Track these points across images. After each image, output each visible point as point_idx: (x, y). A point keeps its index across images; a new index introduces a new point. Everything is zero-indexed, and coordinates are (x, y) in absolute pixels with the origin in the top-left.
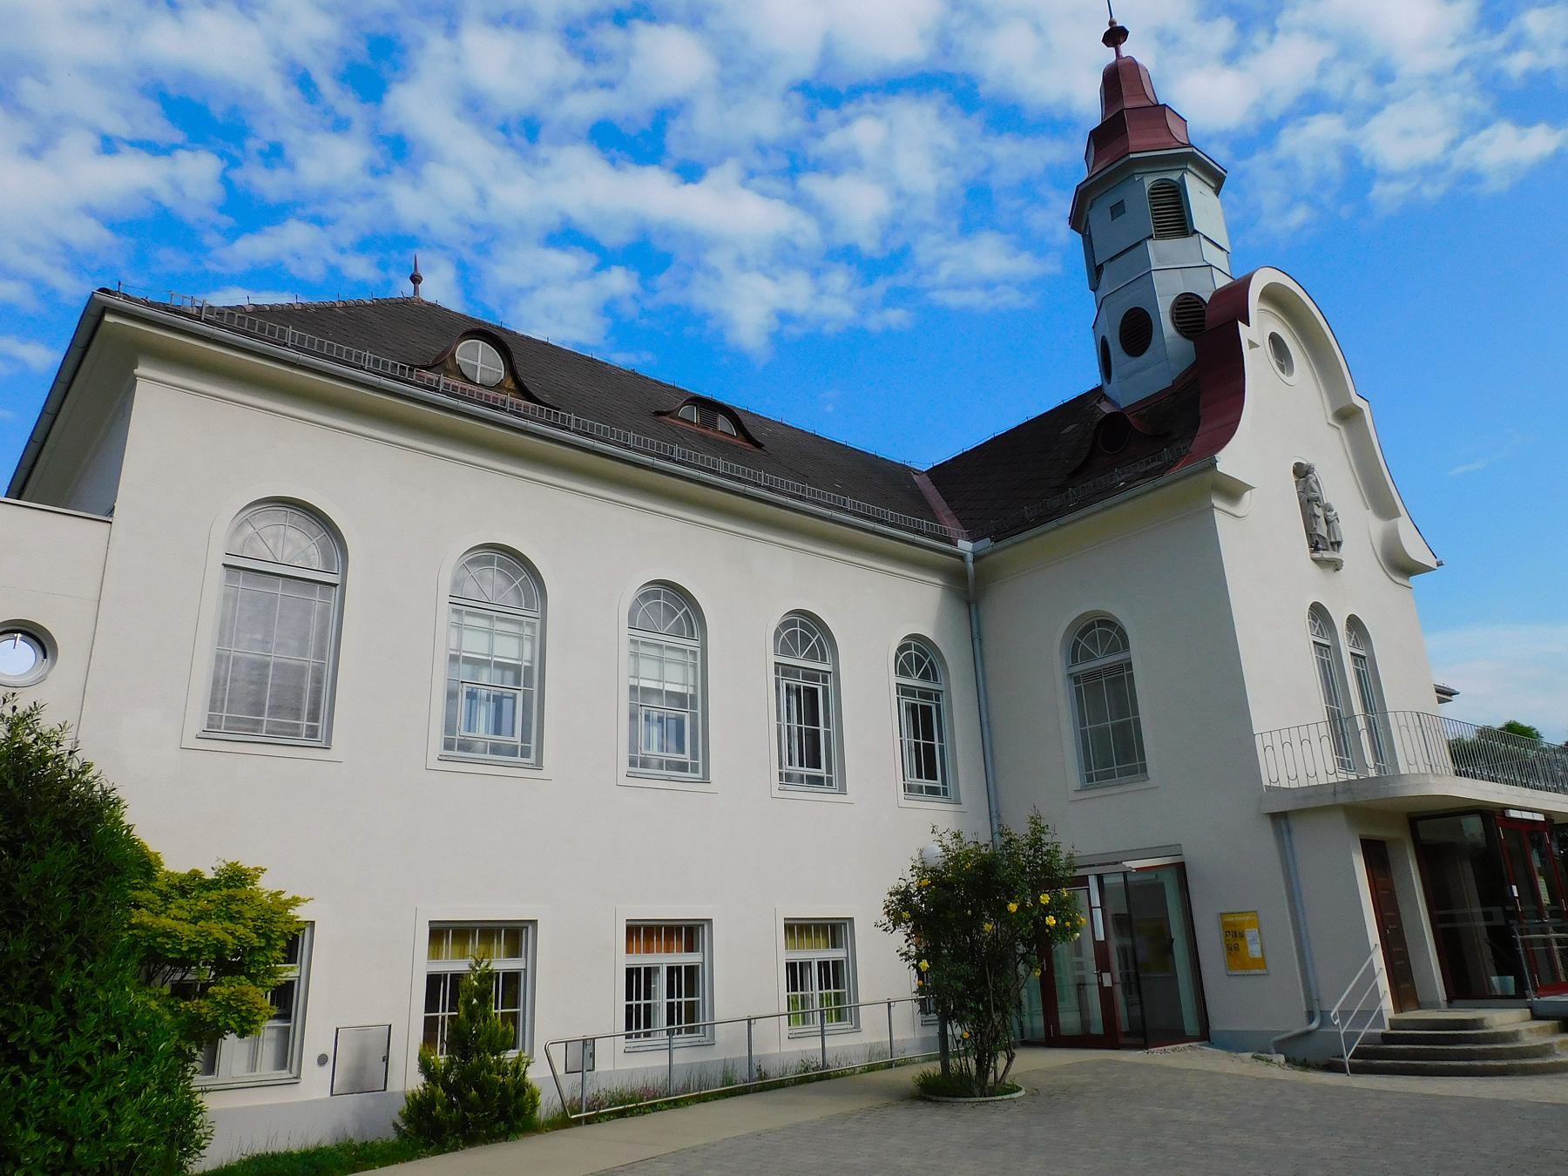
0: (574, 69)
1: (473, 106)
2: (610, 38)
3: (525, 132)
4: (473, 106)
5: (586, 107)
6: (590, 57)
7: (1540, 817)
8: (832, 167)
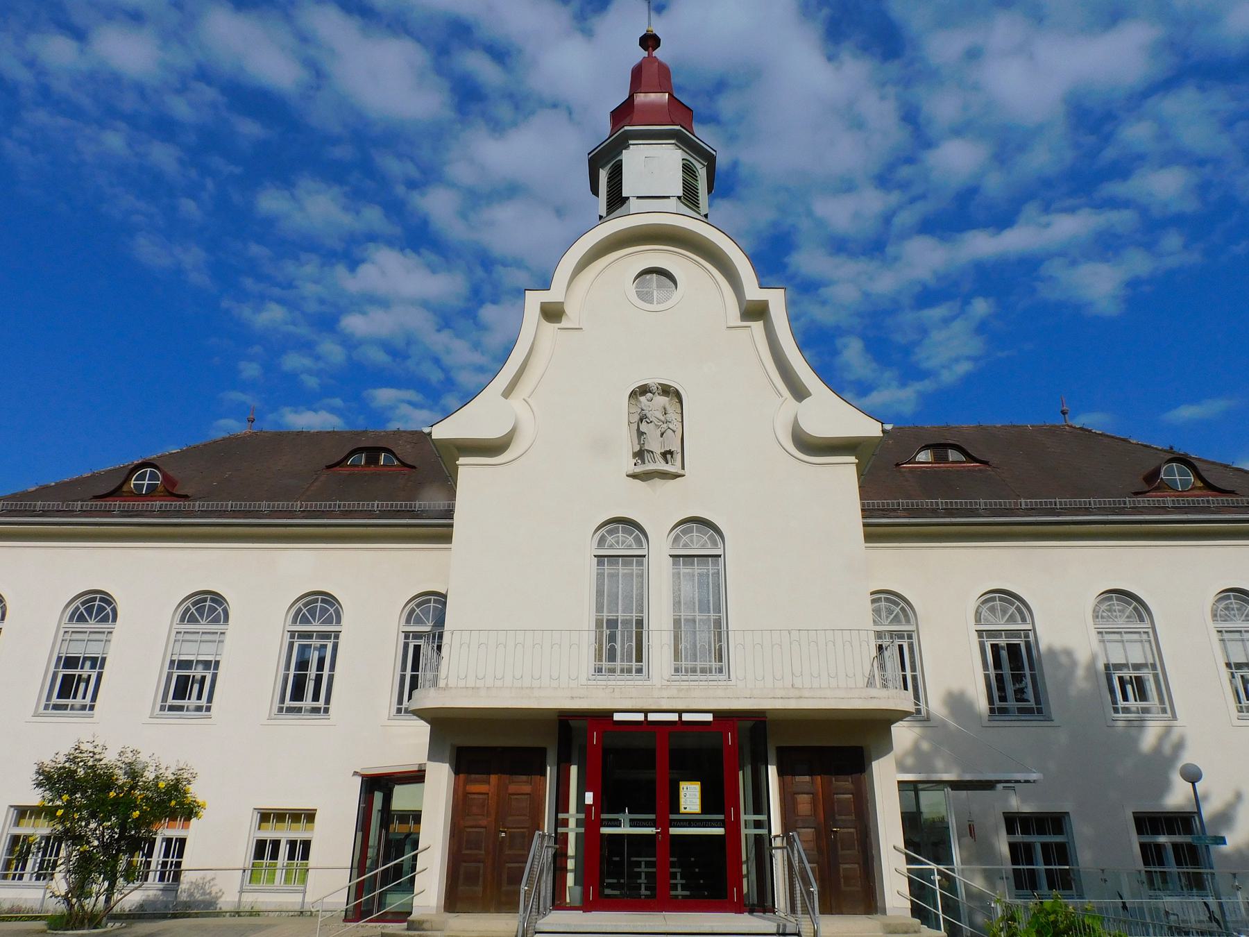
0: (894, 198)
1: (840, 246)
2: (905, 172)
3: (876, 246)
4: (840, 246)
5: (906, 218)
6: (904, 186)
7: (709, 717)
8: (1122, 169)
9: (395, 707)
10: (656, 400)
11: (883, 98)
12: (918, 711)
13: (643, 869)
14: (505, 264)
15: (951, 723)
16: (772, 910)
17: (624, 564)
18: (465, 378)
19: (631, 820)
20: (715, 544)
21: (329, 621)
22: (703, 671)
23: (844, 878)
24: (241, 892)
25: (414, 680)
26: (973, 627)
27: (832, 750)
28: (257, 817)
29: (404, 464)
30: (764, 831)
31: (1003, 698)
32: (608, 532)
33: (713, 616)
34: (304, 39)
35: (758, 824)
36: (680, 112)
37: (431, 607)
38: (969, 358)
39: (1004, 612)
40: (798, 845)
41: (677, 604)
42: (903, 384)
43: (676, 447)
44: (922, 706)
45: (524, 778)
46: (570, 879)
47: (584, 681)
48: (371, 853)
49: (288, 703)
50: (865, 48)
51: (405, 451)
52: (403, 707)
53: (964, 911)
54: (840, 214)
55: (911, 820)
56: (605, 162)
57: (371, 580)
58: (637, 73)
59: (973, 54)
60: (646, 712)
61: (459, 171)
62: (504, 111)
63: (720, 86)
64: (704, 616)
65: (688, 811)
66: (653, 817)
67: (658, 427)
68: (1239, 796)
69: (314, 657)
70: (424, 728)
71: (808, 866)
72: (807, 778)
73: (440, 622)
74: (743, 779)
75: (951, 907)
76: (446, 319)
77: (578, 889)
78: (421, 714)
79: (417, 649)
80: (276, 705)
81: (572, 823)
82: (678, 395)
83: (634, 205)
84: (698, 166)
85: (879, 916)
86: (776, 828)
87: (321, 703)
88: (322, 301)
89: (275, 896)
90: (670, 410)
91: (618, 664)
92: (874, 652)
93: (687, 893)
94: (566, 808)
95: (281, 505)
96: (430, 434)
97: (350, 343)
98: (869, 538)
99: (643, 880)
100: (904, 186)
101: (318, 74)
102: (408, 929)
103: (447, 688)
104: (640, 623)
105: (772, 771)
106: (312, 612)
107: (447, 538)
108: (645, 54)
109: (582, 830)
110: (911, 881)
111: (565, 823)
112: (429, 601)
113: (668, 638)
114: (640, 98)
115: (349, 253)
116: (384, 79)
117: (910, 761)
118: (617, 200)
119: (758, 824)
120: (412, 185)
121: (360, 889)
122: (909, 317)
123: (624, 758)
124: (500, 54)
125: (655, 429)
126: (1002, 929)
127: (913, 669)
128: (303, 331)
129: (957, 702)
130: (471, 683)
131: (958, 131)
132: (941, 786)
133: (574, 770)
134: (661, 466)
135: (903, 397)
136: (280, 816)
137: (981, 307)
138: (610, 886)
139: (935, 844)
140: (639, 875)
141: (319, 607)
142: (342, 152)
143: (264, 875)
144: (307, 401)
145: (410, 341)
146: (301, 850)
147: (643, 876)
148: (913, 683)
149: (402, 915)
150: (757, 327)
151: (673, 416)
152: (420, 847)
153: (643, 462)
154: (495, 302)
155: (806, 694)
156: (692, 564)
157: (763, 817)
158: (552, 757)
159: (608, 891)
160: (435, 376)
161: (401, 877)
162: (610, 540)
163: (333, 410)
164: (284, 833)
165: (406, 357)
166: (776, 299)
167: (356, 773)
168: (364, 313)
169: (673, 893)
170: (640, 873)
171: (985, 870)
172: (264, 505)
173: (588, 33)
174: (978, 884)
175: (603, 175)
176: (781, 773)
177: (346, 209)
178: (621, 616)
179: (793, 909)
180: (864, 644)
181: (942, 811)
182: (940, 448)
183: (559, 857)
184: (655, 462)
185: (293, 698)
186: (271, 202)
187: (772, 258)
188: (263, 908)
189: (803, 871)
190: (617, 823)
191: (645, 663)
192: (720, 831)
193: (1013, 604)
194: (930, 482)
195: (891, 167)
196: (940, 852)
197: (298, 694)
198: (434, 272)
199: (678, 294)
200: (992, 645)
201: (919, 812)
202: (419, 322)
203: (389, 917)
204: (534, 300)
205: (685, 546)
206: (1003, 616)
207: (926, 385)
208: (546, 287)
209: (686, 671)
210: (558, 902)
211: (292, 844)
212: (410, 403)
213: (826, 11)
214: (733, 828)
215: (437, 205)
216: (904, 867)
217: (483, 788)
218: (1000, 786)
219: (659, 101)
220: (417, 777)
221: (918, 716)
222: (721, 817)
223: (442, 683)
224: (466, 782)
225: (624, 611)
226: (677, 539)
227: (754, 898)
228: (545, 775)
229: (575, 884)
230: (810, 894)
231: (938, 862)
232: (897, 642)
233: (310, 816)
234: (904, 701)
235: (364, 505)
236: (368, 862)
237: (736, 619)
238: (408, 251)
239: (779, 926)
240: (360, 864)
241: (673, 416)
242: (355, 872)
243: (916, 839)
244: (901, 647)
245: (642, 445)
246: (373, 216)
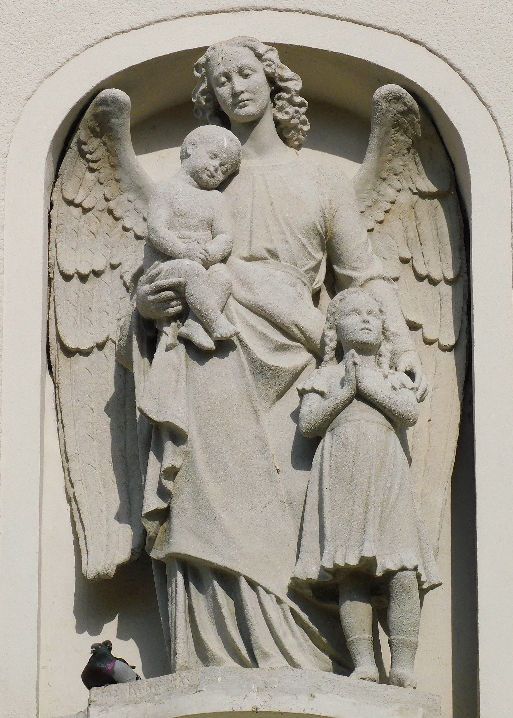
43: (410, 541)
68: (120, 264)
82: (431, 140)
90: (367, 257)
151: (392, 300)
165: (386, 338)
245: (150, 523)
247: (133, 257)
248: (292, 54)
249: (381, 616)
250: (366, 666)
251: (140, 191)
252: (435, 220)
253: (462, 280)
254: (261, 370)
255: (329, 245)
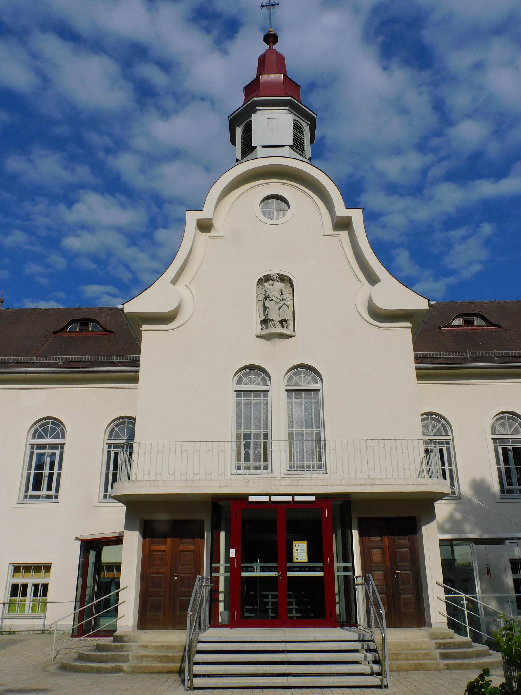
0: (429, 158)
1: (392, 189)
2: (435, 142)
3: (417, 189)
4: (392, 189)
5: (436, 172)
6: (435, 150)
7: (312, 498)
9: (102, 494)
10: (275, 285)
11: (420, 94)
12: (453, 493)
13: (270, 599)
14: (171, 202)
15: (475, 500)
16: (356, 625)
17: (254, 397)
18: (145, 277)
19: (261, 567)
20: (316, 382)
21: (57, 437)
22: (308, 467)
23: (404, 606)
24: (3, 618)
25: (115, 475)
26: (490, 437)
27: (395, 520)
28: (12, 569)
29: (106, 330)
30: (350, 574)
31: (510, 484)
32: (243, 375)
33: (315, 430)
34: (35, 56)
35: (346, 569)
36: (291, 86)
37: (124, 428)
38: (481, 262)
39: (511, 426)
40: (372, 582)
41: (291, 423)
42: (436, 279)
43: (289, 317)
44: (456, 489)
45: (189, 540)
46: (221, 606)
47: (229, 475)
48: (88, 591)
49: (30, 492)
50: (407, 62)
51: (106, 321)
52: (108, 494)
53: (483, 625)
54: (392, 168)
55: (448, 565)
56: (240, 122)
57: (84, 409)
58: (262, 60)
59: (479, 66)
60: (270, 495)
61: (140, 142)
62: (169, 103)
63: (312, 86)
64: (309, 431)
65: (299, 560)
66: (276, 565)
67: (277, 303)
69: (47, 461)
70: (122, 508)
71: (378, 596)
72: (378, 538)
73: (131, 437)
74: (336, 539)
75: (474, 622)
76: (133, 239)
77: (227, 613)
78: (119, 498)
79: (116, 454)
80: (23, 494)
81: (222, 570)
82: (290, 282)
83: (260, 152)
84: (304, 124)
85: (426, 628)
86: (358, 572)
87: (53, 492)
88: (49, 228)
89: (24, 621)
90: (285, 292)
91: (252, 463)
92: (423, 454)
93: (299, 615)
94: (218, 560)
95: (22, 359)
96: (122, 310)
97: (70, 256)
98: (420, 377)
99: (270, 607)
100: (435, 150)
101: (46, 81)
102: (114, 641)
103: (136, 481)
104: (266, 436)
105: (355, 534)
106: (45, 431)
107: (135, 380)
108: (268, 47)
109: (228, 574)
110: (448, 605)
111: (217, 570)
112: (124, 423)
113: (285, 446)
114: (264, 78)
115: (68, 196)
116: (90, 83)
117: (448, 526)
118: (248, 149)
119: (346, 569)
120: (109, 151)
121: (81, 616)
122: (440, 236)
123: (256, 526)
124: (166, 65)
125: (276, 304)
126: (503, 636)
127: (450, 464)
128: (37, 248)
129: (479, 487)
130: (152, 478)
131: (468, 116)
132: (468, 542)
133: (223, 534)
134: (279, 330)
135: (439, 287)
136: (27, 568)
137: (487, 229)
138: (248, 611)
139: (465, 581)
140: (267, 603)
141: (50, 427)
142: (62, 130)
143: (18, 607)
144: (44, 296)
145: (109, 255)
146: (42, 590)
147: (270, 604)
148: (448, 473)
149: (110, 632)
150: (344, 235)
151: (287, 295)
152: (121, 587)
153: (267, 327)
154: (165, 227)
155: (377, 482)
156: (301, 396)
157: (349, 564)
158: (208, 525)
159: (247, 614)
160: (127, 276)
161: (109, 607)
162: (245, 380)
163: (58, 300)
164: (30, 579)
166: (357, 216)
167: (77, 539)
168: (78, 236)
169: (289, 615)
170: (268, 602)
171: (496, 597)
172: (11, 359)
173: (225, 52)
174: (493, 606)
175: (239, 131)
176: (361, 535)
177: (65, 167)
178: (253, 431)
179: (369, 625)
180: (416, 449)
181: (469, 558)
182: (468, 317)
183: (214, 593)
184: (275, 326)
185: (34, 489)
186: (15, 164)
187: (352, 196)
188: (18, 629)
189: (375, 598)
190: (252, 570)
191: (269, 463)
192: (320, 574)
193: (516, 421)
194: (462, 339)
195: (426, 138)
196: (467, 586)
197: (37, 486)
198: (125, 208)
199: (290, 213)
200: (502, 448)
201: (453, 560)
202: (115, 241)
203: (102, 634)
204: (192, 218)
205: (296, 384)
206: (510, 429)
207: (452, 280)
208: (200, 209)
209: (297, 468)
210: (214, 623)
211: (36, 586)
212: (109, 294)
213: (381, 38)
214: (329, 571)
215: (126, 164)
216: (443, 596)
217: (162, 547)
218: (507, 542)
219: (274, 82)
220: (118, 540)
221: (454, 496)
222: (321, 564)
223: (133, 478)
224: (150, 545)
225: (255, 428)
226: (290, 379)
227: (344, 618)
228: (203, 538)
229: (225, 610)
230: (380, 614)
231: (466, 592)
232: (439, 447)
233: (47, 568)
234: (444, 487)
235: (79, 358)
236: (87, 598)
237: (331, 432)
238: (107, 194)
239: (359, 636)
240: (81, 600)
241: (287, 295)
242: (78, 604)
243: (452, 577)
244: (441, 451)
245: (266, 316)
246: (83, 172)
247: (264, 292)
248: (278, 274)
249: (286, 323)
250: (285, 328)
251: (265, 286)
252: (291, 289)
253: (293, 294)
254: (276, 302)
255: (281, 291)
